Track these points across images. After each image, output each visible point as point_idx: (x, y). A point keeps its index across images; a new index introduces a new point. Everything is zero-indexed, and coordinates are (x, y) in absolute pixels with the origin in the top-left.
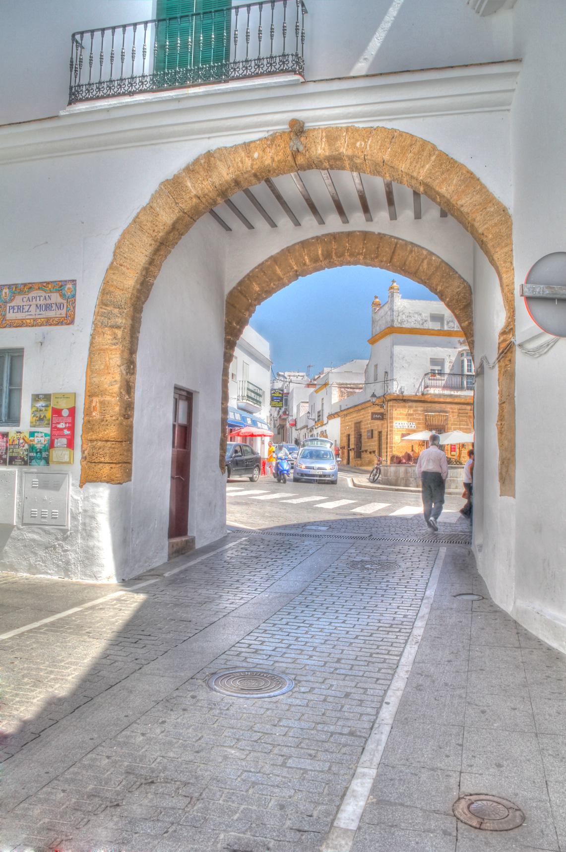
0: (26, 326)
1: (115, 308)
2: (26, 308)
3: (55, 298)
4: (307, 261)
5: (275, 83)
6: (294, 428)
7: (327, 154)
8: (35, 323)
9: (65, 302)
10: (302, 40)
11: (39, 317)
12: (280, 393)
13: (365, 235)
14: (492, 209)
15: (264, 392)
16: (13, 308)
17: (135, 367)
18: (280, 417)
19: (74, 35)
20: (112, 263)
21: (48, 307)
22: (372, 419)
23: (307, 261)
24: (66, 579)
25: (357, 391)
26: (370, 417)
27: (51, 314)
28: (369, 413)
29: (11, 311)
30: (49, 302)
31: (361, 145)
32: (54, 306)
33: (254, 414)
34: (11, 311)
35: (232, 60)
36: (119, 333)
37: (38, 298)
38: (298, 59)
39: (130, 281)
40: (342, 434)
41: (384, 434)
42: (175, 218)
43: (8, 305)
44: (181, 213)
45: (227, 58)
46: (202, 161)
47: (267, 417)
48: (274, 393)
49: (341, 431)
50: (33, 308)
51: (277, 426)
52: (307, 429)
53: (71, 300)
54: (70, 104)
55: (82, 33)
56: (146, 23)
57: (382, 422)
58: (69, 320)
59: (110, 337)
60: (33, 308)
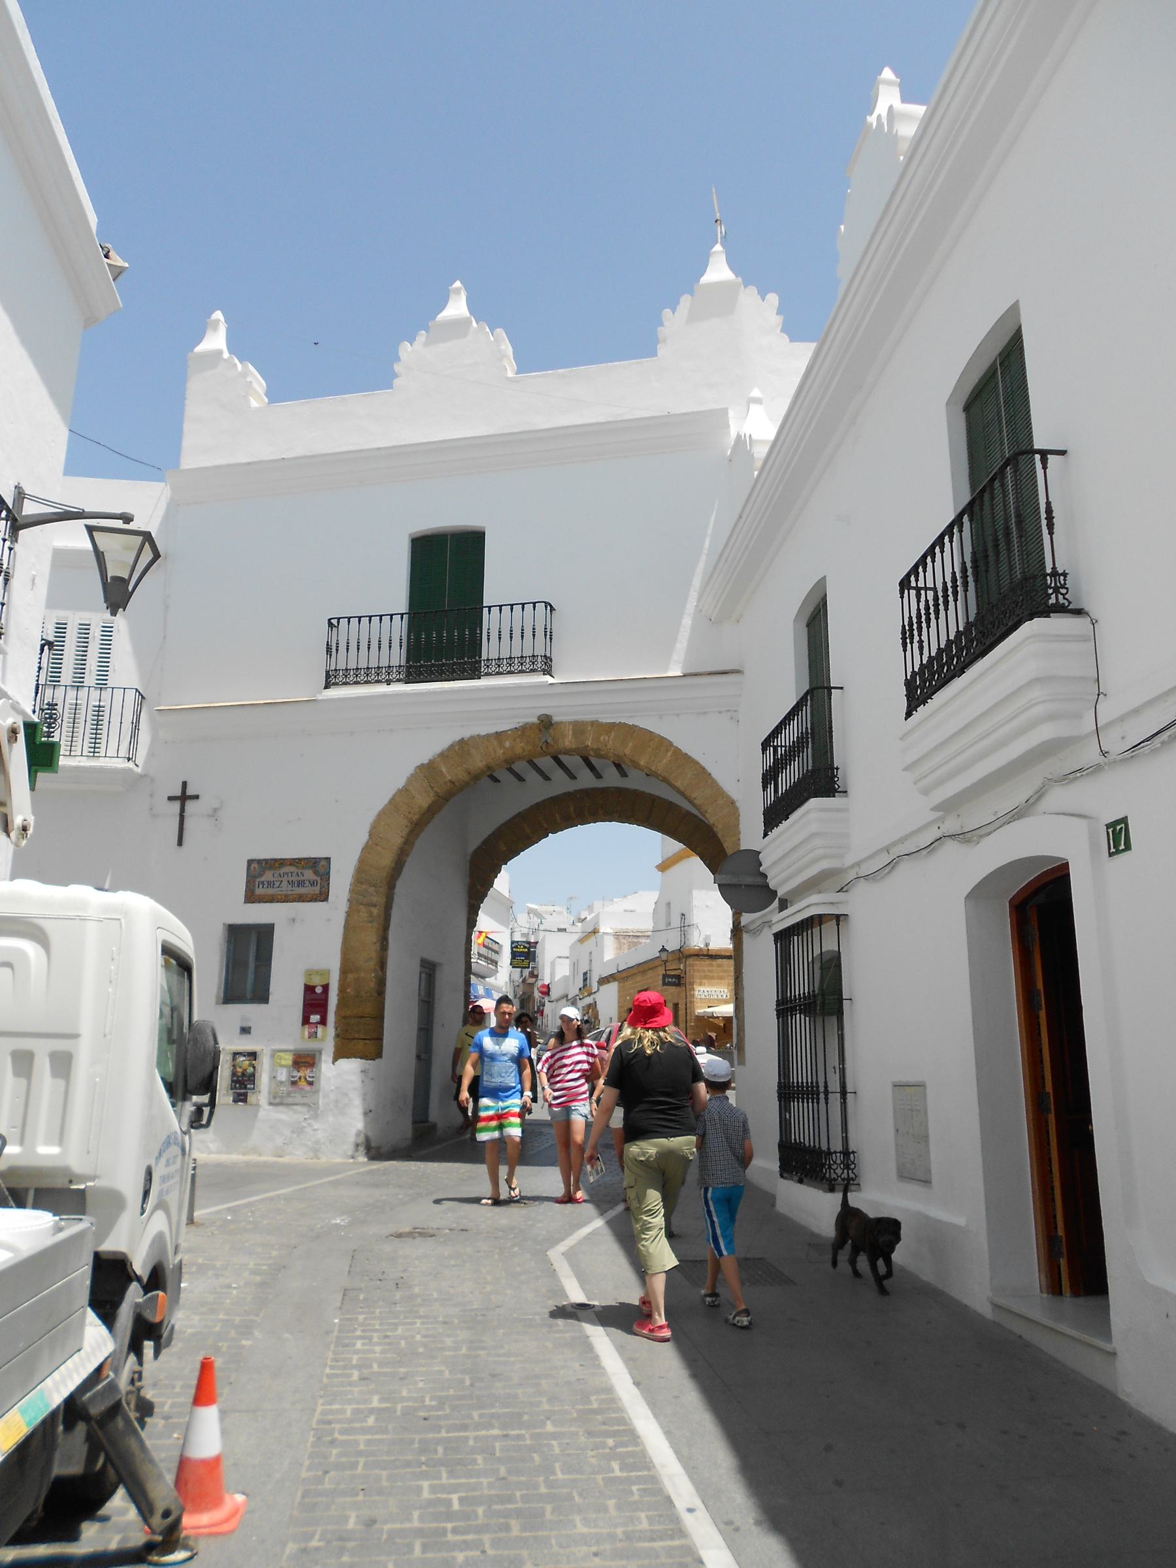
0: (277, 902)
1: (371, 886)
2: (277, 884)
3: (309, 874)
4: (558, 819)
5: (526, 683)
6: (546, 999)
7: (574, 746)
8: (286, 899)
9: (319, 879)
10: (551, 639)
11: (291, 892)
12: (525, 947)
13: (620, 791)
14: (722, 802)
15: (501, 947)
16: (263, 882)
17: (387, 942)
18: (524, 981)
19: (329, 620)
20: (368, 842)
21: (301, 883)
22: (664, 984)
23: (558, 819)
24: (315, 1161)
25: (643, 940)
26: (661, 982)
27: (301, 890)
28: (659, 975)
29: (261, 886)
30: (301, 878)
31: (604, 739)
32: (307, 883)
33: (487, 979)
34: (261, 886)
35: (484, 657)
36: (375, 911)
37: (290, 875)
38: (548, 659)
39: (387, 859)
40: (620, 1007)
41: (682, 1007)
42: (430, 802)
43: (257, 880)
44: (437, 798)
45: (480, 657)
46: (457, 748)
47: (506, 983)
48: (516, 947)
49: (619, 1002)
50: (285, 883)
51: (518, 996)
52: (567, 1000)
53: (325, 877)
54: (326, 687)
55: (339, 619)
56: (402, 615)
57: (679, 989)
58: (323, 896)
59: (366, 915)
60: (285, 883)
